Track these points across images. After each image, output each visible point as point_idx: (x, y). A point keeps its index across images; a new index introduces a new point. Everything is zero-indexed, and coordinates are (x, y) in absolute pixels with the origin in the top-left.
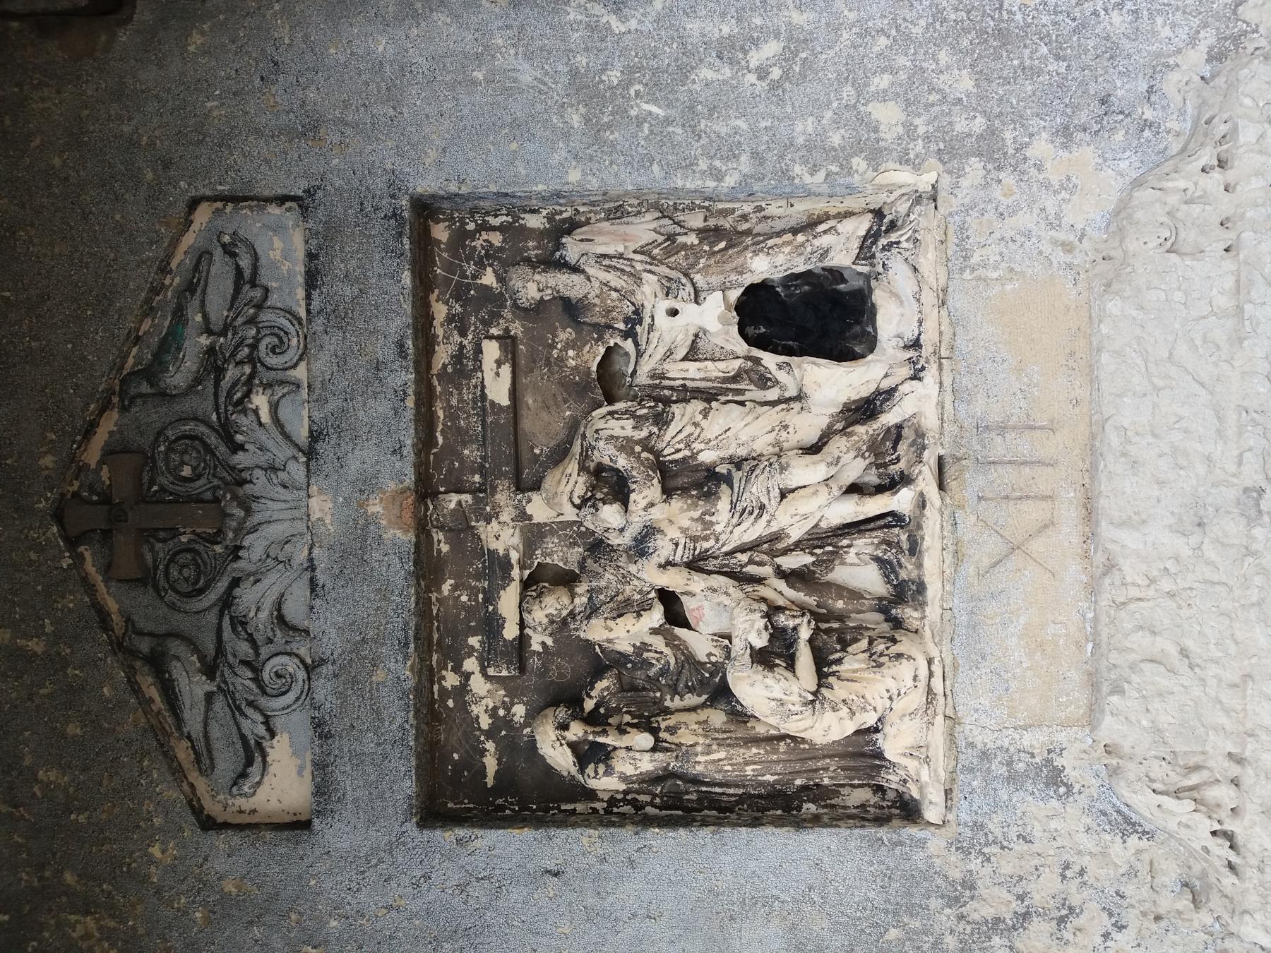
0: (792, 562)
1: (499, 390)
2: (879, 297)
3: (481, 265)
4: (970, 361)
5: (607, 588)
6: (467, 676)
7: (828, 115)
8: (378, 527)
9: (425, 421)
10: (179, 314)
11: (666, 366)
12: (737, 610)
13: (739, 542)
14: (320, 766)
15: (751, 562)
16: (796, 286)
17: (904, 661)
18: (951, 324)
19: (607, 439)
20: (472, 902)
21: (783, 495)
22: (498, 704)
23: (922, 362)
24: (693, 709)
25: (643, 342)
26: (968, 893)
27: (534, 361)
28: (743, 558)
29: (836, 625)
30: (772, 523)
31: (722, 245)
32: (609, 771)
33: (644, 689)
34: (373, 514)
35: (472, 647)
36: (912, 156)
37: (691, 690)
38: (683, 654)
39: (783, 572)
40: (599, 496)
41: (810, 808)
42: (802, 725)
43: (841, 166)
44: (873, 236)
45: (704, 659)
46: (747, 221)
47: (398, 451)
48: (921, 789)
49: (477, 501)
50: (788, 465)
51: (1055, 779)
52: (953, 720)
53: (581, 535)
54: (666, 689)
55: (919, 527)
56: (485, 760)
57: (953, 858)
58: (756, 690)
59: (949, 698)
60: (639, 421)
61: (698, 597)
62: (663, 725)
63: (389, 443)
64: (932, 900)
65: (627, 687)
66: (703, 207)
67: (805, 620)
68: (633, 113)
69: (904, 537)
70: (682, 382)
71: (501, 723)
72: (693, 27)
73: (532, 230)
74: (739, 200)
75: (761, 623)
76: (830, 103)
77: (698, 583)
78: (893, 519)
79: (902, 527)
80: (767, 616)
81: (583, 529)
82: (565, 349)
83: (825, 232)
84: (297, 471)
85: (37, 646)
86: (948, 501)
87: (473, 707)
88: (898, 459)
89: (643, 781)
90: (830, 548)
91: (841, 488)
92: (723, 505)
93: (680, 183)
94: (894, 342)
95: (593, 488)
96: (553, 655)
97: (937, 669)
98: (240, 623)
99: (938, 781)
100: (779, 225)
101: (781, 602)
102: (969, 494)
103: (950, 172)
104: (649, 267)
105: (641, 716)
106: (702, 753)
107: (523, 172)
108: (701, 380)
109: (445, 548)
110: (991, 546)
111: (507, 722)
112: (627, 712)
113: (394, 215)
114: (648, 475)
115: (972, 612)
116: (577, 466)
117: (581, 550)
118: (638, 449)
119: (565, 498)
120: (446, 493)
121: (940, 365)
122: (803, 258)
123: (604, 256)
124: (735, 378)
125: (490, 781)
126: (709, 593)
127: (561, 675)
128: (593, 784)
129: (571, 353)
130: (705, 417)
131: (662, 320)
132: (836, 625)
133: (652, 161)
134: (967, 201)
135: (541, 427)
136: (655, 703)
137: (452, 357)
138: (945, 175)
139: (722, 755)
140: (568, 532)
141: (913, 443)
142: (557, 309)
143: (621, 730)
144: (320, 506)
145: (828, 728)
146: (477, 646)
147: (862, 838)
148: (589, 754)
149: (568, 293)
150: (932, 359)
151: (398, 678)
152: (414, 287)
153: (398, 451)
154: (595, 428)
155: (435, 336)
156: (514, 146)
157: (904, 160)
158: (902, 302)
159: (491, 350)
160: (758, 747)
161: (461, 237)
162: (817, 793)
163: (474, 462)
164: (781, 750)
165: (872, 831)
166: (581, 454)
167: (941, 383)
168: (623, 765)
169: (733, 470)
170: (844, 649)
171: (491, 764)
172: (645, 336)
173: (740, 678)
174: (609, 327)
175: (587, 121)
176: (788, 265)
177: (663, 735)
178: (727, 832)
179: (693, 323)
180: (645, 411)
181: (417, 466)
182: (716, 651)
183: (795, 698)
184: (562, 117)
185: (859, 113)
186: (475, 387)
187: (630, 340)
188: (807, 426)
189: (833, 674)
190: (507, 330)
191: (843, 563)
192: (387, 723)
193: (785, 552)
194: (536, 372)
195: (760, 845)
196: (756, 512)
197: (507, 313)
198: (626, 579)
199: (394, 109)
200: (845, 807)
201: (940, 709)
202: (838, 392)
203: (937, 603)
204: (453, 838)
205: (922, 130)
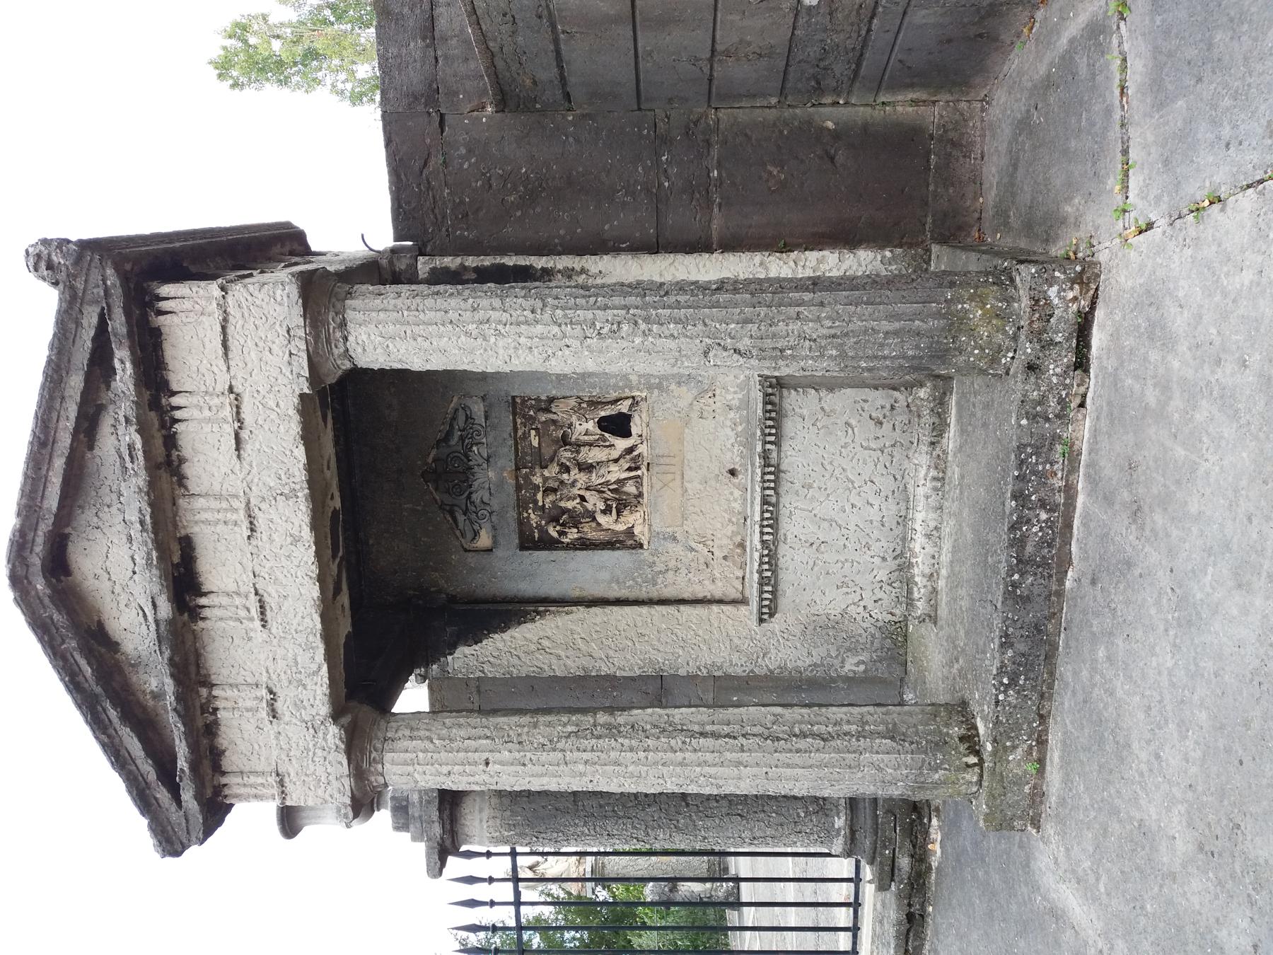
1: (535, 443)
10: (451, 425)
14: (494, 537)
51: (675, 539)
52: (650, 525)
58: (602, 519)
65: (570, 517)
71: (539, 526)
84: (485, 466)
110: (661, 484)
135: (547, 452)
144: (491, 474)
145: (620, 527)
148: (561, 533)
159: (533, 432)
162: (620, 542)
168: (570, 536)
179: (585, 427)
188: (615, 454)
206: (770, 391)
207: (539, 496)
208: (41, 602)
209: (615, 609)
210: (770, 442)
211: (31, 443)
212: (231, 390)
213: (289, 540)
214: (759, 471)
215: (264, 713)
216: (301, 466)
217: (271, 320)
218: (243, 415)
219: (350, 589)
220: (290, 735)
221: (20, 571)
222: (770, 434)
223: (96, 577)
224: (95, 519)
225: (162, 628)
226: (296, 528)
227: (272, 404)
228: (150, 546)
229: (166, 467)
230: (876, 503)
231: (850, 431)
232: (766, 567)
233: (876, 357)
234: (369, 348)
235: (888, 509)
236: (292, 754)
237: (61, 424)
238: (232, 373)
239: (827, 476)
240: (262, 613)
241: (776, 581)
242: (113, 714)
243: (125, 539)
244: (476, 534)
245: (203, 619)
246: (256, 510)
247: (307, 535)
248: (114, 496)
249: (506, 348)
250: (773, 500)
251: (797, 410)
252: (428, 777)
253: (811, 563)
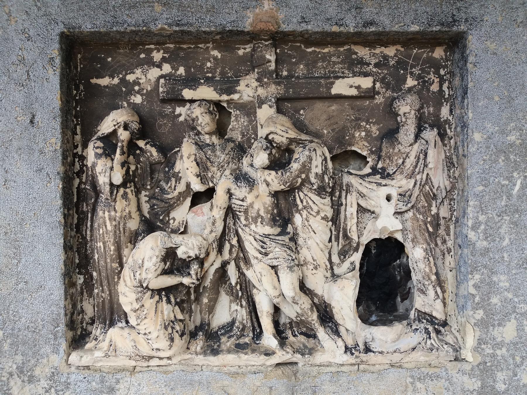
0: (232, 272)
1: (342, 87)
2: (398, 327)
3: (419, 78)
4: (356, 382)
5: (215, 156)
6: (159, 66)
7: (510, 296)
8: (255, 7)
11: (354, 194)
12: (200, 239)
13: (244, 239)
15: (232, 246)
16: (400, 272)
17: (169, 343)
18: (379, 371)
19: (310, 156)
20: (13, 68)
21: (273, 267)
22: (142, 86)
23: (357, 353)
24: (139, 208)
25: (370, 179)
26: (26, 379)
27: (358, 110)
28: (234, 242)
29: (192, 297)
30: (256, 261)
31: (431, 229)
32: (98, 156)
33: (152, 178)
34: (263, 4)
35: (178, 69)
36: (483, 346)
37: (152, 207)
38: (174, 203)
39: (226, 266)
40: (274, 151)
41: (81, 280)
42: (127, 279)
43: (478, 303)
44: (432, 320)
45: (171, 216)
46: (442, 243)
47: (304, 20)
48: (91, 350)
49: (271, 73)
50: (292, 271)
53: (249, 140)
54: (152, 192)
55: (253, 351)
56: (107, 78)
57: (47, 370)
58: (149, 251)
59: (147, 369)
60: (320, 177)
61: (210, 212)
62: (128, 190)
63: (309, 15)
64: (21, 357)
65: (153, 167)
66: (452, 217)
67: (194, 281)
68: (515, 174)
69: (247, 340)
70: (344, 203)
71: (130, 88)
73: (440, 110)
74: (456, 238)
75: (192, 254)
76: (517, 296)
77: (218, 214)
78: (258, 334)
79: (253, 338)
80: (197, 258)
81: (253, 141)
82: (366, 130)
83: (436, 292)
86: (270, 369)
87: (140, 70)
88: (295, 336)
89: (93, 177)
90: (240, 294)
91: (278, 304)
92: (268, 230)
93: (471, 203)
94: (369, 336)
95: (279, 148)
96: (173, 121)
97: (165, 362)
99: (95, 362)
100: (439, 263)
101: (206, 265)
102: (273, 382)
103: (472, 370)
104: (418, 183)
105: (134, 176)
106: (110, 215)
107: (480, 104)
108: (345, 215)
109: (241, 52)
111: (130, 92)
112: (137, 167)
113: (455, 21)
114: (287, 183)
115: (200, 383)
116: (293, 137)
117: (239, 139)
118: (303, 176)
119: (272, 129)
120: (276, 53)
121: (354, 365)
122: (421, 279)
123: (426, 155)
124: (346, 236)
125: (94, 81)
126: (211, 220)
127: (160, 126)
128: (91, 145)
129: (363, 134)
130: (323, 218)
131: (384, 191)
132: (192, 297)
133: (485, 186)
134: (455, 380)
135: (317, 114)
136: (143, 185)
137: (362, 58)
138: (471, 367)
139: (109, 228)
140: (251, 131)
141: (305, 347)
142: (391, 125)
143: (123, 164)
145: (127, 297)
146: (179, 73)
147: (59, 315)
148: (109, 143)
149: (402, 131)
150: (358, 360)
151: (157, 20)
152: (408, 33)
153: (304, 20)
154: (317, 149)
155: (375, 48)
156: (497, 99)
157: (480, 342)
158: (395, 342)
159: (366, 83)
160: (115, 250)
161: (436, 65)
162: (89, 285)
163: (295, 71)
164: (113, 265)
165: (63, 321)
166: (300, 140)
167: (342, 365)
169: (289, 236)
170: (177, 303)
171: (105, 81)
172: (374, 181)
173: (156, 240)
174: (379, 158)
175: (511, 145)
176: (417, 270)
177: (122, 190)
178: (60, 231)
180: (327, 181)
181: (293, 33)
182: (176, 223)
183: (144, 276)
184: (514, 129)
185: (510, 314)
186: (343, 73)
187: (370, 171)
188: (317, 282)
189: (161, 298)
190: (378, 93)
191: (231, 302)
192: (127, 12)
193: (238, 267)
194: (351, 112)
195: (53, 251)
196: (263, 251)
197: (389, 93)
198: (221, 168)
199: (521, 22)
200: (81, 301)
201: (139, 363)
202: (338, 301)
203: (205, 362)
204: (54, 55)
205: (499, 352)
207: (206, 92)
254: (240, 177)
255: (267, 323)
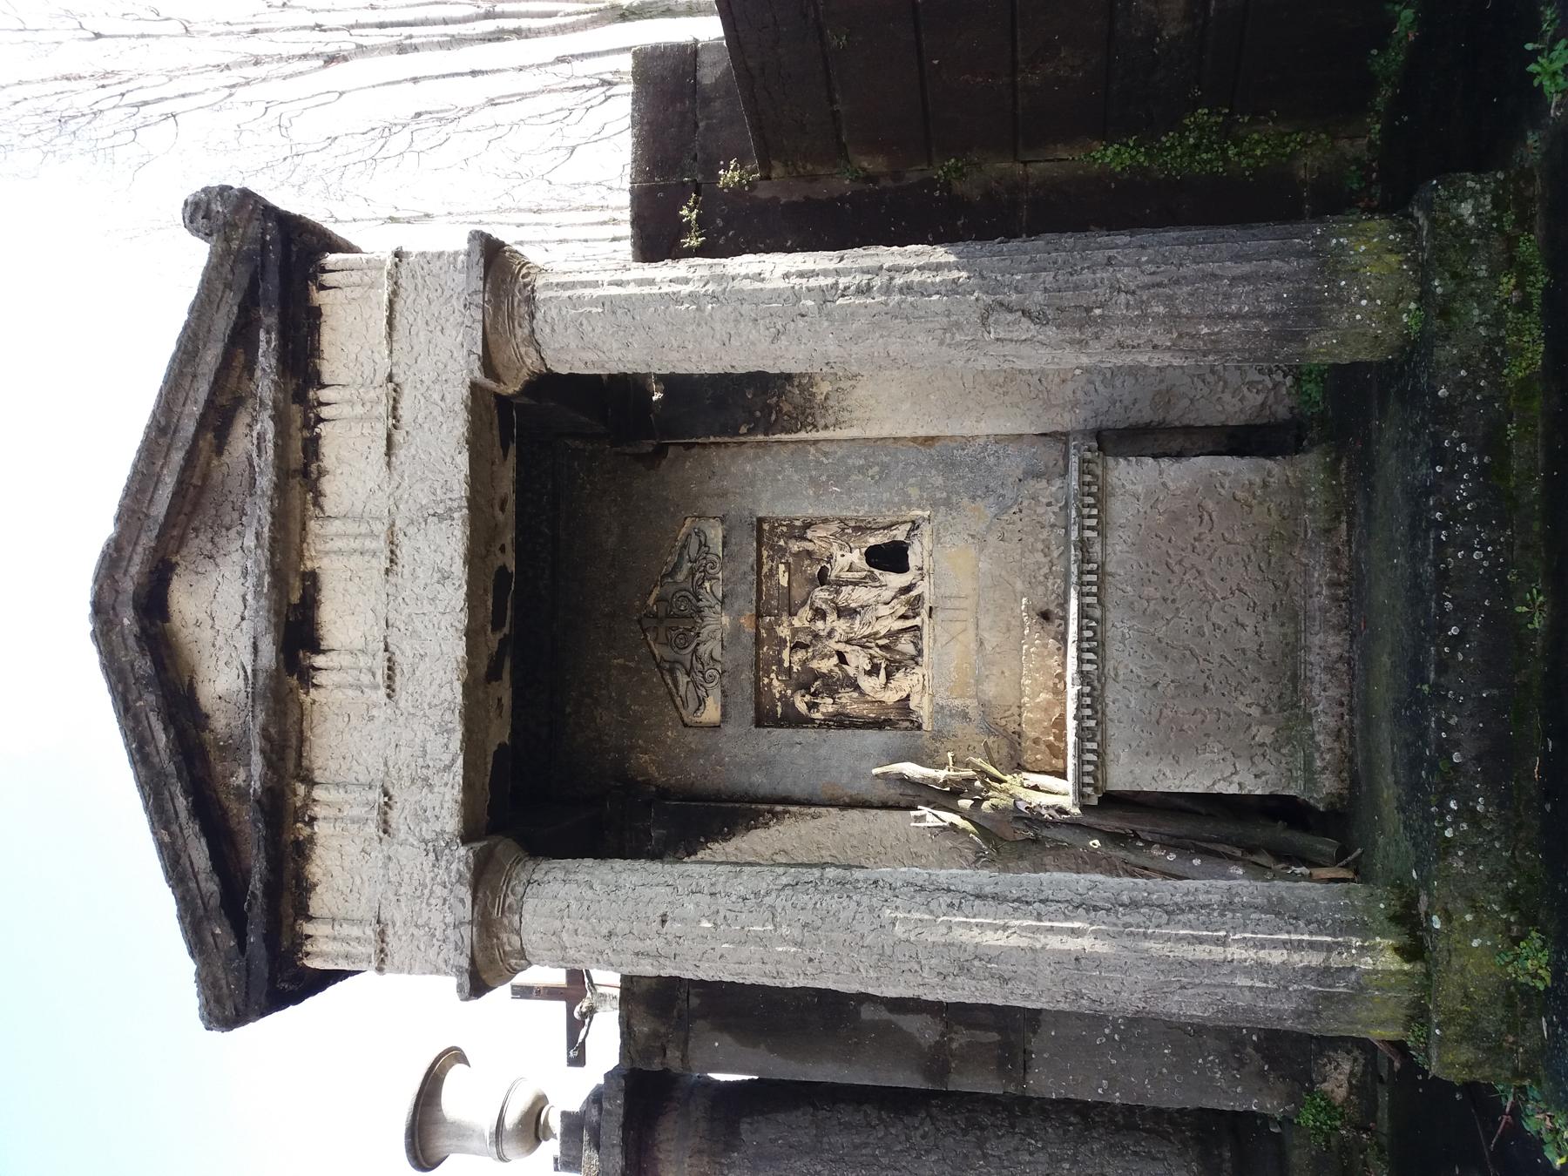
0: (881, 642)
9: (759, 591)
10: (681, 555)
14: (723, 706)
58: (867, 683)
71: (783, 696)
72: (850, 461)
77: (848, 648)
78: (916, 628)
84: (718, 608)
85: (632, 664)
98: (699, 658)
135: (798, 594)
145: (891, 697)
148: (812, 706)
157: (919, 507)
161: (773, 528)
171: (779, 710)
206: (1089, 455)
207: (786, 654)
208: (124, 640)
209: (880, 812)
210: (1089, 528)
211: (148, 427)
212: (390, 378)
213: (437, 576)
214: (1074, 568)
215: (372, 829)
216: (462, 477)
217: (447, 293)
218: (400, 412)
219: (512, 673)
220: (404, 861)
221: (108, 599)
222: (1090, 517)
223: (198, 624)
224: (209, 546)
225: (261, 678)
226: (447, 560)
227: (436, 397)
228: (263, 567)
229: (300, 472)
230: (1250, 622)
231: (1206, 517)
232: (1088, 712)
233: (1221, 316)
234: (559, 328)
235: (1266, 632)
236: (402, 891)
237: (187, 410)
238: (395, 359)
239: (1176, 582)
240: (389, 677)
241: (1104, 733)
242: (182, 803)
243: (239, 573)
244: (701, 702)
245: (316, 686)
246: (401, 536)
247: (459, 571)
248: (236, 515)
249: (724, 321)
250: (1097, 613)
251: (1129, 487)
252: (581, 940)
253: (1156, 713)
254: (830, 635)
255: (909, 623)
